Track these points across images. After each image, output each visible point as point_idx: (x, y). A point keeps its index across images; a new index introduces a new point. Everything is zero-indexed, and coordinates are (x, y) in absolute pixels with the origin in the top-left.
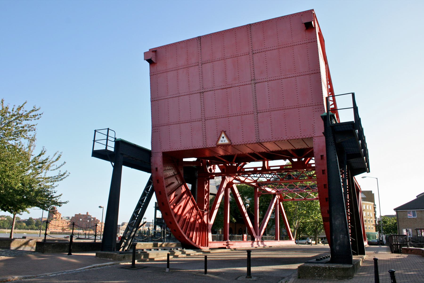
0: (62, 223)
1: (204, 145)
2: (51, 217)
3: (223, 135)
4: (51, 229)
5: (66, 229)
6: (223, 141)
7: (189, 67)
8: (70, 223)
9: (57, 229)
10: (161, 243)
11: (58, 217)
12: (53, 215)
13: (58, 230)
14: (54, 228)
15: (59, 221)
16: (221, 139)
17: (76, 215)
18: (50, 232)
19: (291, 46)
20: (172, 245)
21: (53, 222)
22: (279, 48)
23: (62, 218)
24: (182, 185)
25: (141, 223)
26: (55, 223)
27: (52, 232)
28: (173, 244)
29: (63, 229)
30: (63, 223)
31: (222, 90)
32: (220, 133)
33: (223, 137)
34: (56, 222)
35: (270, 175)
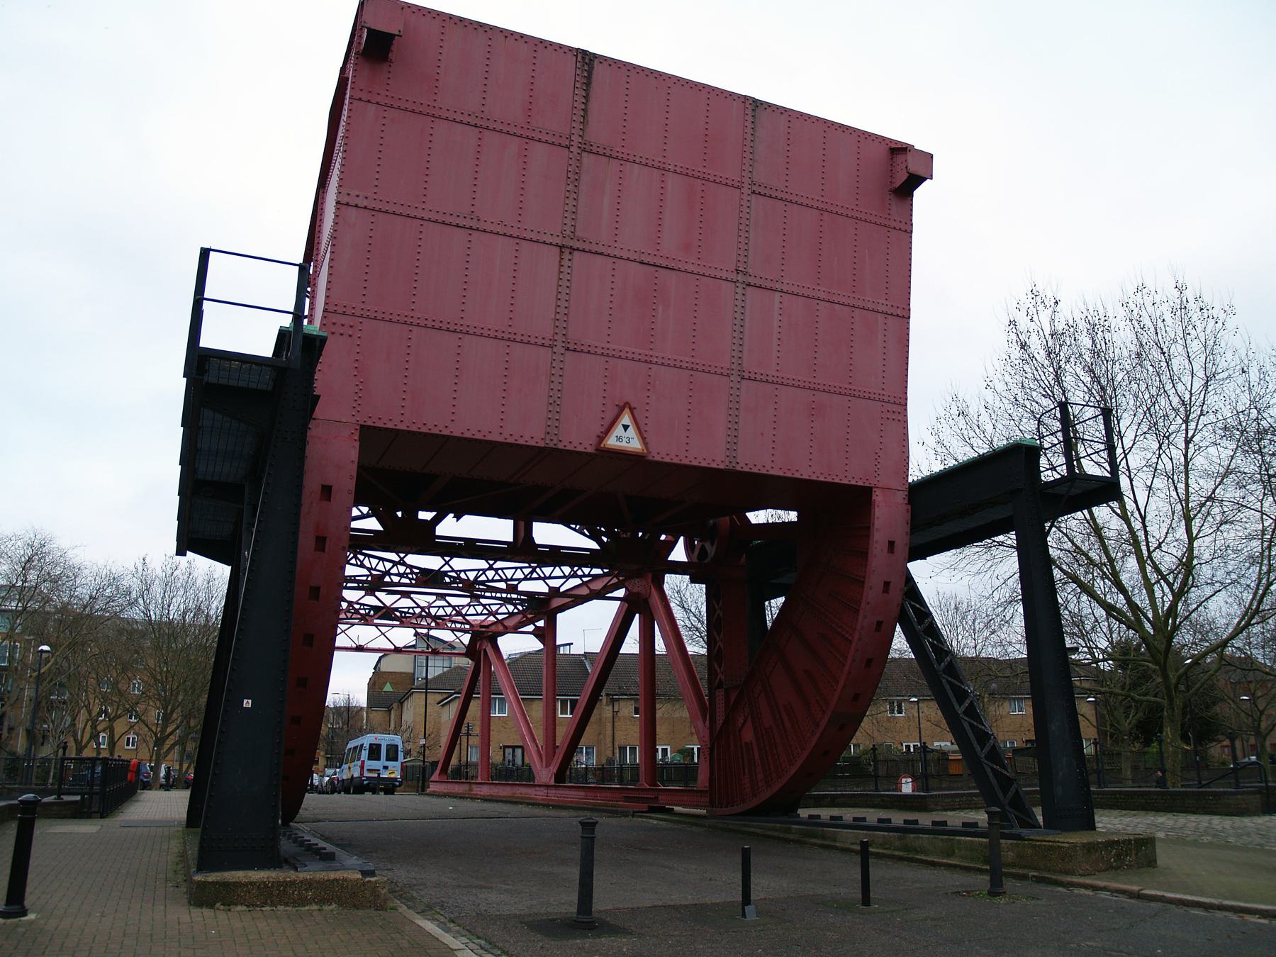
1: (548, 437)
3: (626, 419)
6: (625, 440)
7: (533, 139)
16: (617, 430)
19: (852, 217)
22: (822, 210)
31: (642, 265)
32: (616, 410)
33: (626, 427)
35: (557, 568)
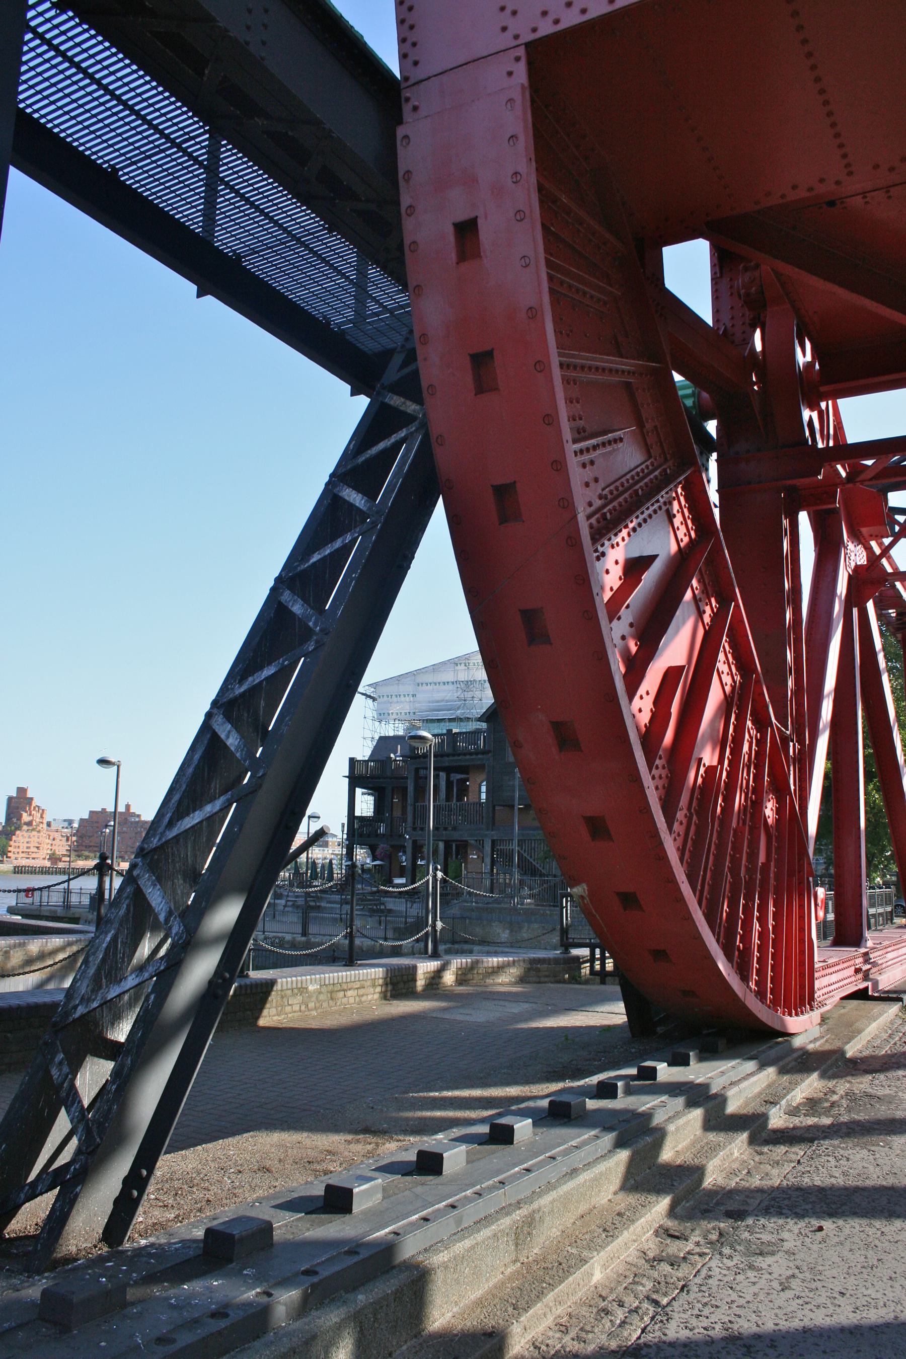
0: (51, 838)
2: (15, 820)
4: (16, 859)
5: (63, 859)
8: (74, 838)
9: (34, 858)
10: (433, 965)
11: (38, 820)
12: (21, 816)
13: (37, 861)
14: (24, 855)
15: (39, 832)
17: (91, 812)
18: (15, 867)
20: (499, 969)
21: (21, 837)
23: (49, 824)
24: (665, 481)
25: (300, 838)
26: (27, 840)
27: (19, 867)
28: (508, 965)
29: (54, 858)
30: (54, 839)
34: (30, 837)
